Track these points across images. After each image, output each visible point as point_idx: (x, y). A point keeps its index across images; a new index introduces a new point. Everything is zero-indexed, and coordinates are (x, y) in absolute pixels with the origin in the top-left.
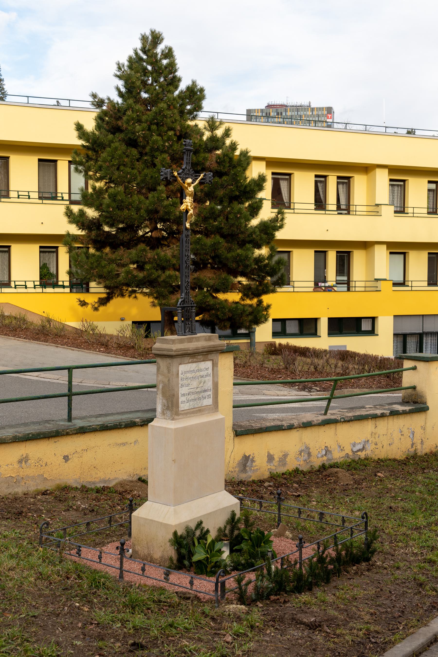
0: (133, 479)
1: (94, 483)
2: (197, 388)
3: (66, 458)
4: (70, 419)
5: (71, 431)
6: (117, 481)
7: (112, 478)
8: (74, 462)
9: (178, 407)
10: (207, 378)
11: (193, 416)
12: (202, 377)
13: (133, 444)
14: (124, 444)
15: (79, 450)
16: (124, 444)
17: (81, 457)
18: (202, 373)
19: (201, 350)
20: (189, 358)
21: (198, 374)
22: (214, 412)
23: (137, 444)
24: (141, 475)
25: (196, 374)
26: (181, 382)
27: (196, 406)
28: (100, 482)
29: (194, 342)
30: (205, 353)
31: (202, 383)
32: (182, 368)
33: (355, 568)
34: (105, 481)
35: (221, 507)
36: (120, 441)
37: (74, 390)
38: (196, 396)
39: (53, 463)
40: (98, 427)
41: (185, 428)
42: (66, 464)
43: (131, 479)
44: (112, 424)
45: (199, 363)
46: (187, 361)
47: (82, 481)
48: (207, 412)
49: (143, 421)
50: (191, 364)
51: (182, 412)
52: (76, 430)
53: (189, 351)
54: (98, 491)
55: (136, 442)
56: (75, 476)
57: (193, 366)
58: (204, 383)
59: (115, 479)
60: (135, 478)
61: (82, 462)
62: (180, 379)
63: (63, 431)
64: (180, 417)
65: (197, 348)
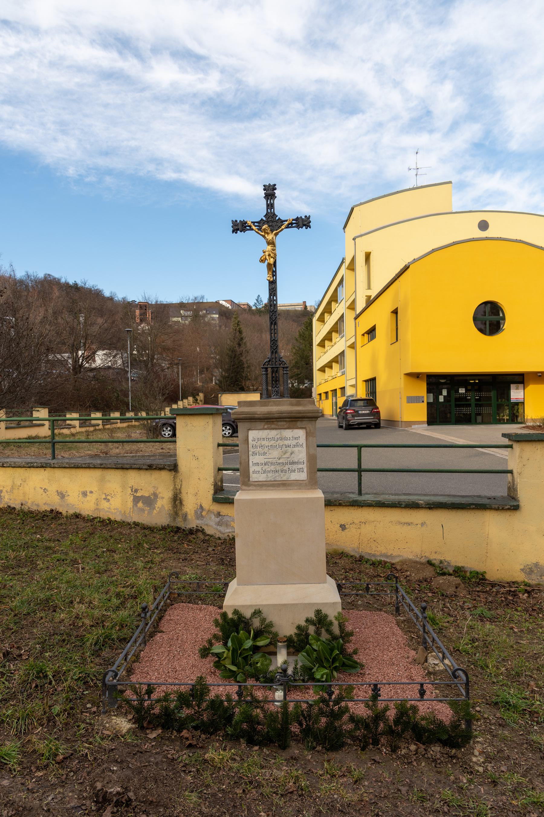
0: (421, 560)
1: (374, 555)
2: (279, 459)
3: (343, 527)
4: (360, 493)
5: (344, 502)
6: (401, 558)
7: (394, 554)
8: (352, 533)
9: (248, 477)
10: (296, 449)
11: (272, 490)
12: (289, 446)
13: (419, 526)
14: (409, 524)
15: (355, 521)
16: (409, 524)
17: (359, 528)
18: (286, 442)
19: (276, 415)
20: (263, 424)
21: (281, 443)
22: (309, 489)
23: (425, 526)
24: (431, 558)
25: (277, 443)
26: (251, 450)
27: (278, 479)
28: (381, 555)
29: (271, 406)
30: (287, 420)
31: (289, 453)
32: (253, 434)
33: (413, 747)
34: (387, 556)
35: (306, 602)
36: (403, 520)
37: (363, 467)
38: (278, 468)
39: (330, 529)
40: (374, 503)
41: (252, 501)
42: (343, 533)
43: (418, 560)
44: (390, 502)
45: (282, 430)
46: (262, 427)
47: (360, 550)
48: (296, 488)
49: (428, 504)
50: (268, 431)
51: (254, 483)
52: (350, 502)
53: (257, 416)
54: (373, 564)
55: (423, 524)
56: (353, 545)
57: (273, 433)
58: (291, 454)
59: (399, 556)
60: (424, 560)
61: (360, 534)
62: (250, 446)
63: (335, 501)
64: (251, 488)
65: (268, 412)
